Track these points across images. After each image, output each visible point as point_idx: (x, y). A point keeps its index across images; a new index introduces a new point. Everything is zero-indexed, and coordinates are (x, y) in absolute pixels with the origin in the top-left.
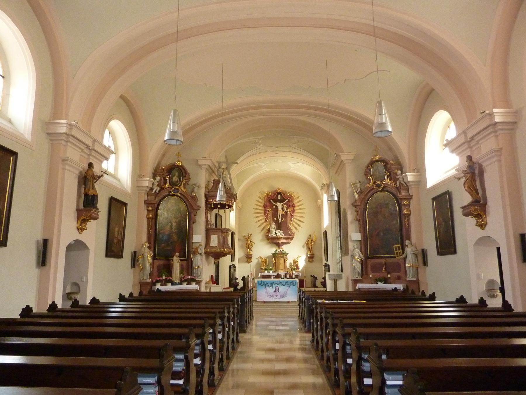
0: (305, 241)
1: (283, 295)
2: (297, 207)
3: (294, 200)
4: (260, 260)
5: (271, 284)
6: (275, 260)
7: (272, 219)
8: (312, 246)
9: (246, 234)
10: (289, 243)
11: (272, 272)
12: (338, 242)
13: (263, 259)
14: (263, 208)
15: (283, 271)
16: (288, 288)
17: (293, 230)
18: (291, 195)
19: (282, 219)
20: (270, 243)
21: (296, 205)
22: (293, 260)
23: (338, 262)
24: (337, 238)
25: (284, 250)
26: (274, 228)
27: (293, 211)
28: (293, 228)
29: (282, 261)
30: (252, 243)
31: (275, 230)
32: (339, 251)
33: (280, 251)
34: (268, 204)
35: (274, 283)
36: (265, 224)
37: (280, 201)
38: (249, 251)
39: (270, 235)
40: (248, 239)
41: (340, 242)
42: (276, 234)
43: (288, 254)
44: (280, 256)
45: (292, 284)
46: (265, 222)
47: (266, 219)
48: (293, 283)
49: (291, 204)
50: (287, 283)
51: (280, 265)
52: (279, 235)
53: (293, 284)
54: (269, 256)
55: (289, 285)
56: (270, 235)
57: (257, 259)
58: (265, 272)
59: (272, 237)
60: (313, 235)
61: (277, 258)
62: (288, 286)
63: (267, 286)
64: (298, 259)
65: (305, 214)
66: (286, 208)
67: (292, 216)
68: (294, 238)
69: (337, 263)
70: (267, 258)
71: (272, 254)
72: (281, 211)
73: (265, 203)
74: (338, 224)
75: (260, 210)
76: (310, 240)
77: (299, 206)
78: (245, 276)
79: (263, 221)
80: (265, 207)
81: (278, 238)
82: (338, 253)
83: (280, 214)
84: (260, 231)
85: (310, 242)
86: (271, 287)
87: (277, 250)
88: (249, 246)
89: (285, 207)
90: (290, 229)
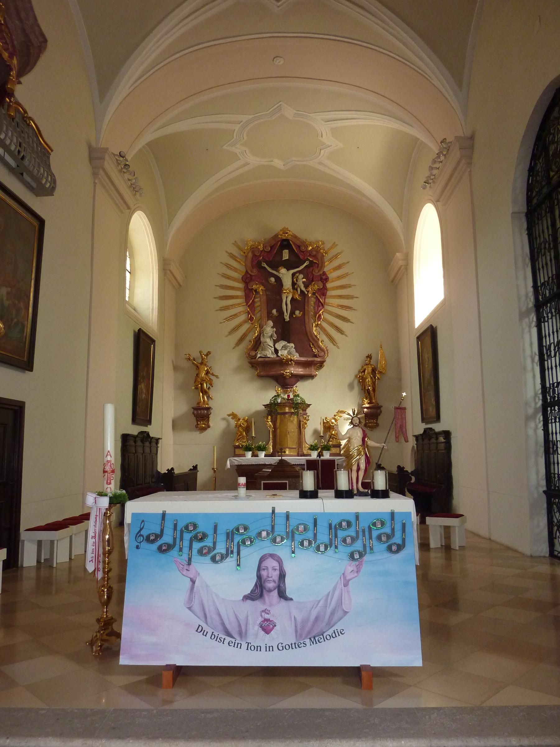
0: (357, 372)
1: (317, 619)
2: (333, 281)
3: (326, 264)
4: (233, 423)
5: (230, 536)
6: (274, 422)
7: (265, 314)
8: (374, 383)
9: (195, 354)
10: (312, 377)
11: (266, 456)
12: (530, 331)
13: (239, 419)
14: (241, 285)
15: (296, 454)
16: (349, 567)
17: (324, 342)
18: (317, 250)
19: (292, 313)
20: (260, 376)
21: (331, 276)
22: (324, 423)
23: (531, 411)
24: (523, 315)
25: (298, 396)
26: (271, 336)
27: (323, 291)
28: (322, 337)
29: (292, 425)
30: (212, 377)
31: (275, 342)
32: (533, 369)
33: (289, 396)
34: (255, 272)
35: (252, 533)
36: (246, 327)
37: (289, 265)
38: (203, 397)
39: (259, 356)
40: (199, 365)
41: (535, 331)
42: (276, 351)
43: (309, 405)
44: (287, 410)
45: (379, 538)
46: (245, 322)
47: (249, 313)
48: (387, 530)
49: (316, 272)
50: (341, 534)
51: (286, 436)
52: (283, 353)
53: (389, 537)
54: (257, 413)
55: (358, 545)
56: (259, 356)
57: (224, 419)
58: (244, 455)
59: (267, 359)
60: (378, 354)
61: (279, 416)
62: (352, 556)
63: (200, 552)
64: (336, 420)
65: (355, 299)
66: (303, 282)
67: (320, 304)
68: (325, 363)
69: (528, 418)
70: (251, 417)
71: (266, 406)
72: (292, 290)
73: (247, 271)
74: (528, 261)
75: (232, 288)
76: (370, 369)
77: (339, 278)
78: (172, 469)
79: (243, 317)
80: (247, 281)
81: (283, 363)
82: (529, 376)
83: (287, 298)
84: (234, 346)
85: (368, 373)
86: (231, 561)
87: (278, 396)
88: (202, 385)
89: (301, 280)
90: (314, 340)
